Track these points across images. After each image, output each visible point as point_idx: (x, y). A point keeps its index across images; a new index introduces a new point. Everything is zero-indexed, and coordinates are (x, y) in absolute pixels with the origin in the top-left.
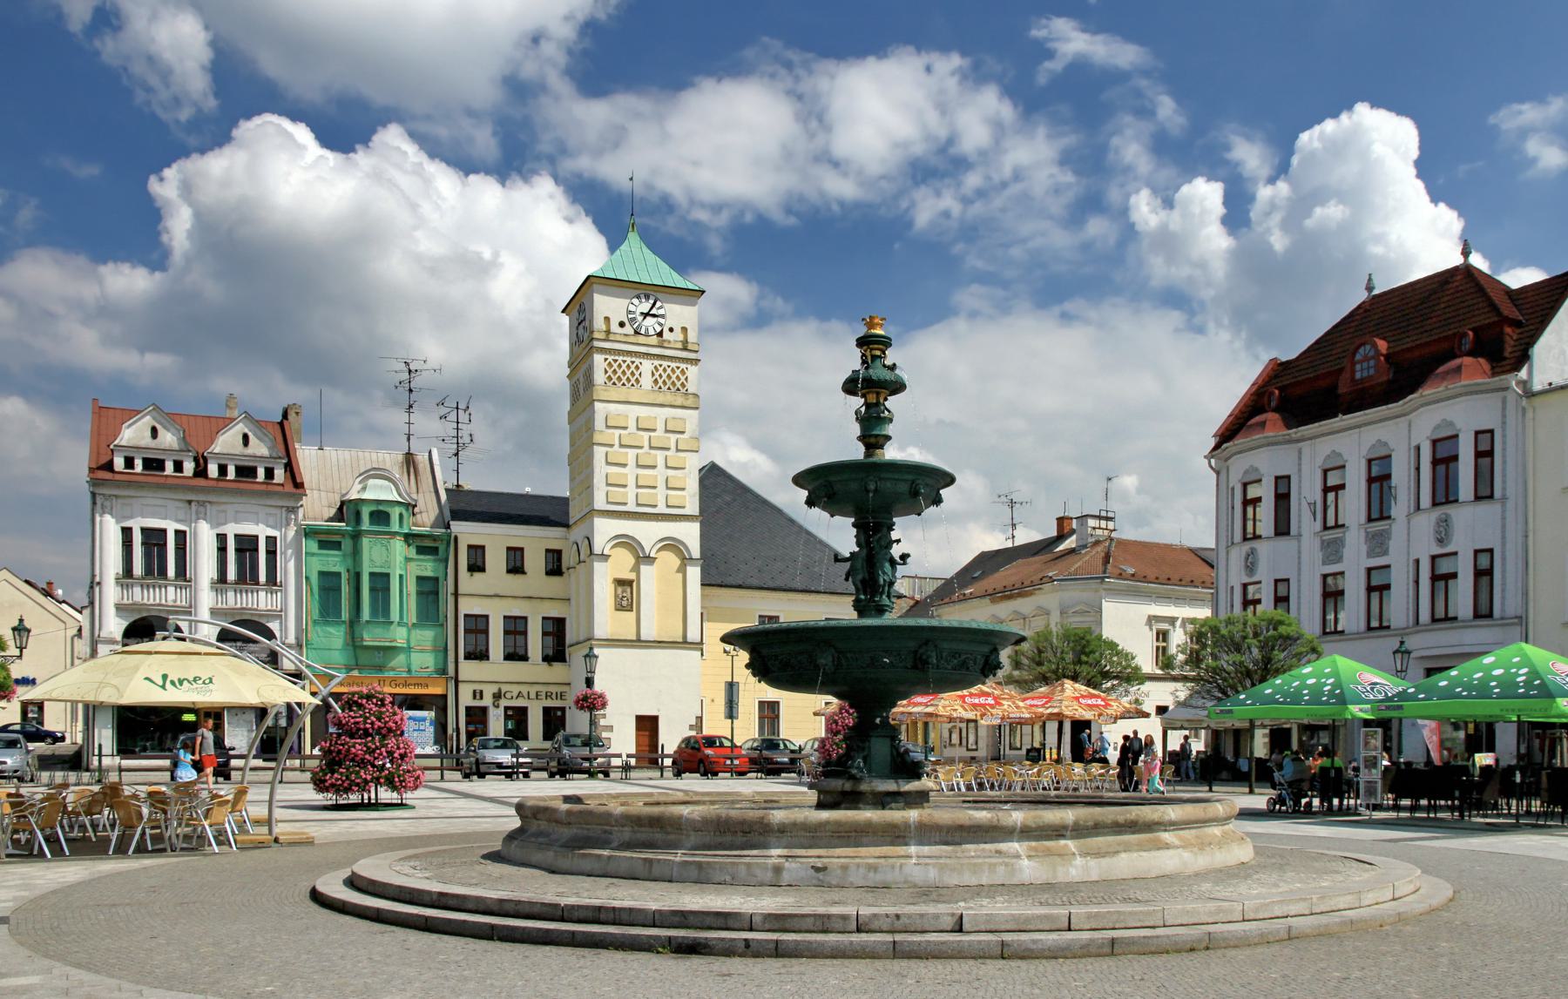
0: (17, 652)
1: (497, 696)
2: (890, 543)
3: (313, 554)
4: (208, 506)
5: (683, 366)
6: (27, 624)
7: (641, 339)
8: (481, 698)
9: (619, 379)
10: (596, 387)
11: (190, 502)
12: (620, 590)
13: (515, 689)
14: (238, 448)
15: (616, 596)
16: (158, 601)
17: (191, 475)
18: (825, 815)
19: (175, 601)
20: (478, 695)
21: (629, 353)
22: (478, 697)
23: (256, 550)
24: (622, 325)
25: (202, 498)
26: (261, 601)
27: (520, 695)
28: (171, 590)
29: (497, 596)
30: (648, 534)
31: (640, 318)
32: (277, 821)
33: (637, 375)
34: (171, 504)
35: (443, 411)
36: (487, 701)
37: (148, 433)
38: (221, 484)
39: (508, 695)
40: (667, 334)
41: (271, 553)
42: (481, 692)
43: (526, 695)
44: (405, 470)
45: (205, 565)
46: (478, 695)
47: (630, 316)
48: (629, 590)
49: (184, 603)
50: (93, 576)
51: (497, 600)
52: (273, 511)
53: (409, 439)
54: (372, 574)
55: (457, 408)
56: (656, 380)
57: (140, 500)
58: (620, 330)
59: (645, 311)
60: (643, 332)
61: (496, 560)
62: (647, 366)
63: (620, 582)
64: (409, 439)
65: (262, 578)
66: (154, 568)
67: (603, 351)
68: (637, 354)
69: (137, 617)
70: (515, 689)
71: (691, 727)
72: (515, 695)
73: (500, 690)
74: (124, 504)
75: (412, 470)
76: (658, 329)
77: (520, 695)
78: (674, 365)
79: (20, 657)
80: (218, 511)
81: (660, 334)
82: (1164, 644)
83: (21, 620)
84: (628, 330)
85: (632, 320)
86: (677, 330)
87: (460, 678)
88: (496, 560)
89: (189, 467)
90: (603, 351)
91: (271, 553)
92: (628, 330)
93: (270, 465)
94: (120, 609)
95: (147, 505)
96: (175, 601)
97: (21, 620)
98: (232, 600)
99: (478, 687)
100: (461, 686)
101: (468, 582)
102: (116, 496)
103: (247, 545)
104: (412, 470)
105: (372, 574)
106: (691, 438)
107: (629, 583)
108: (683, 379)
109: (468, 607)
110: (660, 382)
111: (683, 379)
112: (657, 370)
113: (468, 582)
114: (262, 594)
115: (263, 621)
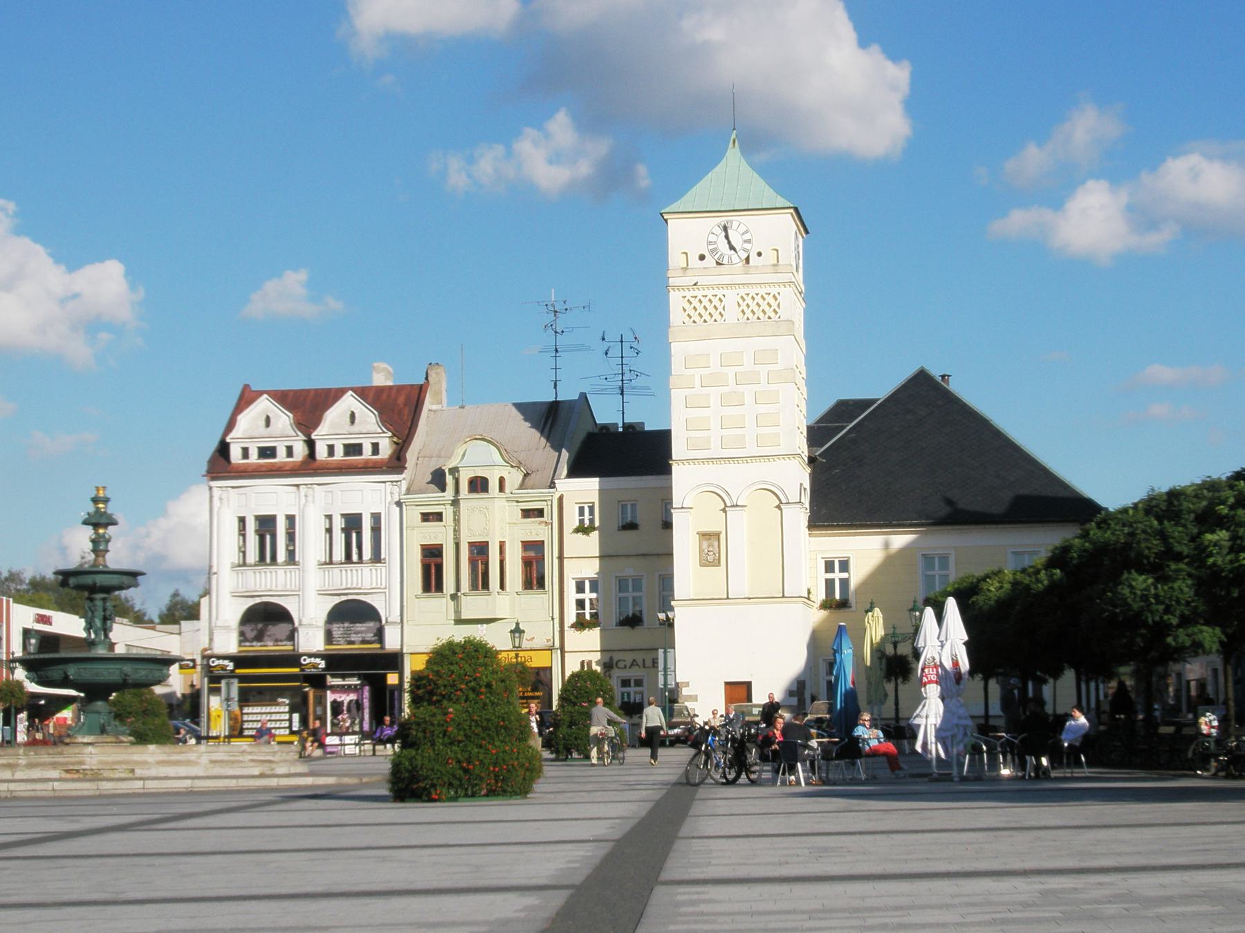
6: (521, 627)
10: (672, 329)
12: (705, 544)
13: (629, 657)
14: (262, 430)
15: (701, 551)
16: (269, 587)
18: (644, 728)
24: (702, 257)
27: (634, 663)
30: (736, 480)
37: (263, 423)
39: (621, 664)
41: (376, 530)
43: (640, 662)
44: (542, 423)
45: (312, 544)
47: (711, 247)
48: (716, 544)
49: (293, 587)
50: (211, 567)
53: (555, 386)
54: (471, 544)
55: (622, 342)
60: (725, 261)
63: (705, 536)
64: (555, 386)
66: (266, 557)
67: (678, 288)
69: (337, 600)
70: (629, 657)
72: (628, 664)
73: (611, 658)
75: (550, 422)
77: (634, 663)
78: (762, 291)
82: (845, 575)
83: (517, 624)
84: (710, 261)
90: (678, 288)
91: (376, 530)
92: (710, 261)
97: (517, 624)
103: (266, 524)
104: (550, 422)
105: (471, 544)
107: (717, 535)
108: (774, 306)
111: (774, 306)
112: (744, 300)
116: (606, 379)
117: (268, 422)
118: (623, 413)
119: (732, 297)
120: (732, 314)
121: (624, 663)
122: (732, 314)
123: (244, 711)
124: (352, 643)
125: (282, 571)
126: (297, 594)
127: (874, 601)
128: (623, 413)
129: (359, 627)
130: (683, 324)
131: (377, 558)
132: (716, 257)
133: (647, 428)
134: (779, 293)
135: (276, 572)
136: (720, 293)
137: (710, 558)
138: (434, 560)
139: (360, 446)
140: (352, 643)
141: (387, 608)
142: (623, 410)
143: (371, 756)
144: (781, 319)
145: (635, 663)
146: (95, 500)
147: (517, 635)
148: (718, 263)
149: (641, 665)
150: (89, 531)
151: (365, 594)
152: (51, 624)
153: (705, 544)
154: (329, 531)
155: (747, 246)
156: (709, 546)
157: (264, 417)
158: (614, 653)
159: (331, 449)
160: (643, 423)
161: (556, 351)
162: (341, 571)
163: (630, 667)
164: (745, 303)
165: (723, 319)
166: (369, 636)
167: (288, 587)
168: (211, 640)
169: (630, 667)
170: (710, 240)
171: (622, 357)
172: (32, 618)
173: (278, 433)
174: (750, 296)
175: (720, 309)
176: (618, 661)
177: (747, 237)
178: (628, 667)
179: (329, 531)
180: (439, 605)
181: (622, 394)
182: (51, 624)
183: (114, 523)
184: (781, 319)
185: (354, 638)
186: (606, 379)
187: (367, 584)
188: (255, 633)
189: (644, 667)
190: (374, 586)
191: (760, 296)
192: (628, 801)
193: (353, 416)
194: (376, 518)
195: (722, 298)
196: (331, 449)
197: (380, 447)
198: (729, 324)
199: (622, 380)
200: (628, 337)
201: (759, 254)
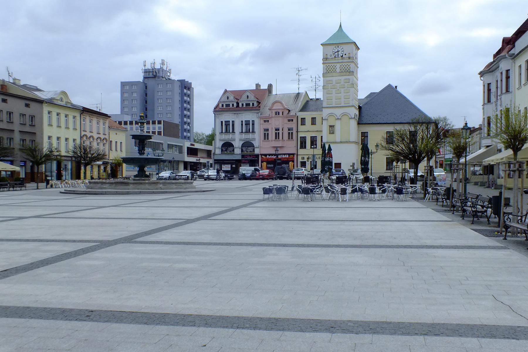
0: (376, 151)
1: (308, 158)
3: (263, 124)
4: (219, 115)
5: (349, 64)
7: (336, 59)
8: (304, 159)
11: (235, 114)
12: (331, 128)
14: (226, 100)
16: (228, 138)
17: (235, 107)
19: (232, 138)
20: (303, 158)
21: (332, 63)
22: (303, 159)
23: (249, 124)
25: (237, 112)
26: (250, 136)
28: (231, 135)
29: (308, 131)
32: (423, 194)
33: (335, 69)
34: (250, 114)
36: (305, 160)
37: (227, 98)
38: (242, 109)
40: (344, 56)
42: (304, 157)
45: (237, 129)
46: (303, 158)
47: (333, 53)
51: (309, 132)
52: (254, 114)
53: (299, 89)
56: (341, 69)
57: (245, 114)
59: (339, 52)
61: (308, 121)
62: (338, 66)
63: (331, 126)
64: (299, 89)
65: (231, 131)
71: (351, 166)
73: (309, 157)
74: (245, 115)
78: (346, 64)
79: (377, 152)
80: (252, 115)
81: (342, 56)
87: (298, 154)
88: (308, 121)
89: (235, 105)
91: (253, 124)
93: (223, 104)
94: (220, 140)
95: (226, 115)
96: (232, 138)
98: (244, 136)
99: (303, 156)
100: (298, 156)
101: (301, 128)
102: (220, 114)
103: (227, 123)
106: (351, 84)
107: (334, 126)
108: (349, 67)
109: (301, 135)
110: (342, 69)
113: (301, 128)
114: (251, 135)
115: (251, 142)
117: (228, 98)
119: (338, 66)
120: (338, 70)
124: (248, 152)
126: (234, 140)
127: (467, 122)
129: (249, 148)
131: (233, 131)
136: (335, 65)
137: (332, 132)
138: (266, 132)
139: (250, 104)
140: (248, 152)
141: (256, 143)
147: (277, 151)
151: (250, 140)
152: (194, 146)
153: (331, 128)
154: (242, 125)
155: (343, 52)
157: (227, 97)
159: (243, 105)
166: (252, 150)
167: (232, 138)
168: (215, 151)
170: (333, 51)
172: (190, 144)
173: (230, 101)
175: (335, 69)
177: (342, 50)
179: (242, 125)
181: (316, 91)
182: (194, 146)
185: (248, 151)
187: (251, 138)
188: (225, 149)
192: (263, 220)
193: (248, 96)
194: (253, 121)
196: (243, 105)
197: (254, 104)
200: (317, 77)
201: (345, 54)
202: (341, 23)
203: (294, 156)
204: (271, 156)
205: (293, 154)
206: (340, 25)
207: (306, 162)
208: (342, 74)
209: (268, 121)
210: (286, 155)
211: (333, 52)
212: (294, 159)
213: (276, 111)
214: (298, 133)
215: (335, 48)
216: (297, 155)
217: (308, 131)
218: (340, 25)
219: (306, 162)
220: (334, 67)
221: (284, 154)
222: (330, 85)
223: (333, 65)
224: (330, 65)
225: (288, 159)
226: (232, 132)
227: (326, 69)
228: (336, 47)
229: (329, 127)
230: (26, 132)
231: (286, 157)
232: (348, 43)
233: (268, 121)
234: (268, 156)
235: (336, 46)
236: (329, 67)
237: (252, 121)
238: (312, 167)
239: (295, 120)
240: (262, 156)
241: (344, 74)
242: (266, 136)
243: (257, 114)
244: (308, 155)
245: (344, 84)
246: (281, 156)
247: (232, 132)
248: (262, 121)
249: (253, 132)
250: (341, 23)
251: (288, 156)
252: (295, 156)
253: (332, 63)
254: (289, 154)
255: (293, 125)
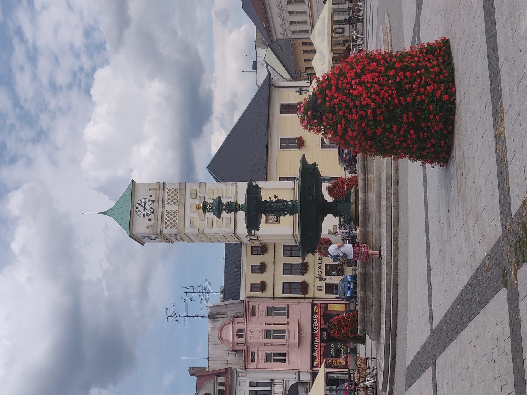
1: (321, 279)
2: (271, 201)
8: (321, 286)
9: (174, 217)
12: (270, 221)
13: (317, 270)
15: (273, 223)
20: (320, 288)
21: (162, 221)
22: (321, 288)
29: (274, 278)
31: (146, 211)
33: (172, 212)
35: (188, 300)
36: (323, 284)
39: (320, 273)
46: (320, 288)
47: (146, 216)
51: (275, 278)
52: (238, 383)
53: (203, 317)
55: (187, 293)
58: (152, 221)
59: (143, 208)
60: (152, 210)
62: (168, 208)
64: (203, 317)
65: (269, 389)
68: (162, 213)
70: (317, 270)
73: (317, 277)
75: (216, 316)
76: (151, 202)
78: (166, 195)
81: (153, 201)
85: (148, 215)
86: (151, 193)
91: (257, 384)
92: (152, 216)
99: (316, 288)
104: (216, 316)
108: (173, 190)
109: (279, 292)
110: (174, 201)
115: (288, 388)
116: (202, 300)
118: (216, 293)
119: (168, 208)
120: (175, 208)
121: (319, 272)
122: (175, 208)
123: (346, 375)
125: (275, 388)
126: (284, 382)
128: (216, 293)
130: (177, 229)
132: (150, 214)
133: (223, 285)
134: (168, 188)
135: (275, 391)
136: (165, 212)
142: (215, 293)
143: (365, 346)
144: (178, 187)
145: (320, 267)
146: (205, 210)
148: (153, 213)
149: (321, 265)
150: (224, 214)
153: (270, 221)
156: (271, 220)
158: (315, 276)
160: (221, 287)
161: (187, 316)
162: (275, 393)
163: (321, 269)
164: (171, 202)
165: (176, 211)
169: (321, 269)
171: (193, 293)
174: (168, 200)
175: (172, 212)
176: (319, 275)
178: (321, 270)
180: (293, 357)
183: (220, 198)
184: (178, 187)
186: (202, 300)
187: (281, 389)
189: (321, 263)
190: (282, 386)
191: (168, 196)
194: (252, 384)
195: (167, 212)
198: (179, 209)
199: (203, 293)
200: (185, 290)
202: (99, 213)
203: (316, 304)
204: (315, 348)
205: (313, 305)
206: (104, 213)
207: (326, 284)
208: (182, 201)
209: (252, 353)
210: (313, 318)
211: (141, 201)
212: (320, 304)
213: (235, 337)
214: (276, 296)
215: (139, 213)
216: (314, 298)
217: (274, 278)
218: (104, 213)
219: (326, 284)
220: (169, 215)
221: (312, 322)
222: (198, 222)
223: (165, 217)
224: (165, 221)
225: (321, 316)
226: (271, 387)
227: (171, 228)
228: (137, 212)
229: (268, 224)
230: (216, 306)
231: (316, 320)
232: (133, 192)
233: (252, 353)
234: (314, 354)
235: (135, 212)
236: (168, 223)
237: (250, 386)
238: (335, 273)
239: (254, 303)
240: (315, 365)
241: (182, 197)
242: (281, 358)
243: (240, 374)
244: (316, 278)
245: (198, 197)
246: (316, 329)
247: (271, 387)
248: (253, 365)
249: (271, 384)
250: (99, 213)
251: (316, 316)
252: (316, 301)
253: (162, 221)
254: (313, 313)
255: (262, 306)
